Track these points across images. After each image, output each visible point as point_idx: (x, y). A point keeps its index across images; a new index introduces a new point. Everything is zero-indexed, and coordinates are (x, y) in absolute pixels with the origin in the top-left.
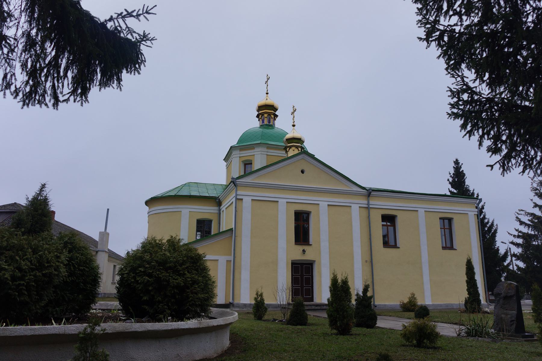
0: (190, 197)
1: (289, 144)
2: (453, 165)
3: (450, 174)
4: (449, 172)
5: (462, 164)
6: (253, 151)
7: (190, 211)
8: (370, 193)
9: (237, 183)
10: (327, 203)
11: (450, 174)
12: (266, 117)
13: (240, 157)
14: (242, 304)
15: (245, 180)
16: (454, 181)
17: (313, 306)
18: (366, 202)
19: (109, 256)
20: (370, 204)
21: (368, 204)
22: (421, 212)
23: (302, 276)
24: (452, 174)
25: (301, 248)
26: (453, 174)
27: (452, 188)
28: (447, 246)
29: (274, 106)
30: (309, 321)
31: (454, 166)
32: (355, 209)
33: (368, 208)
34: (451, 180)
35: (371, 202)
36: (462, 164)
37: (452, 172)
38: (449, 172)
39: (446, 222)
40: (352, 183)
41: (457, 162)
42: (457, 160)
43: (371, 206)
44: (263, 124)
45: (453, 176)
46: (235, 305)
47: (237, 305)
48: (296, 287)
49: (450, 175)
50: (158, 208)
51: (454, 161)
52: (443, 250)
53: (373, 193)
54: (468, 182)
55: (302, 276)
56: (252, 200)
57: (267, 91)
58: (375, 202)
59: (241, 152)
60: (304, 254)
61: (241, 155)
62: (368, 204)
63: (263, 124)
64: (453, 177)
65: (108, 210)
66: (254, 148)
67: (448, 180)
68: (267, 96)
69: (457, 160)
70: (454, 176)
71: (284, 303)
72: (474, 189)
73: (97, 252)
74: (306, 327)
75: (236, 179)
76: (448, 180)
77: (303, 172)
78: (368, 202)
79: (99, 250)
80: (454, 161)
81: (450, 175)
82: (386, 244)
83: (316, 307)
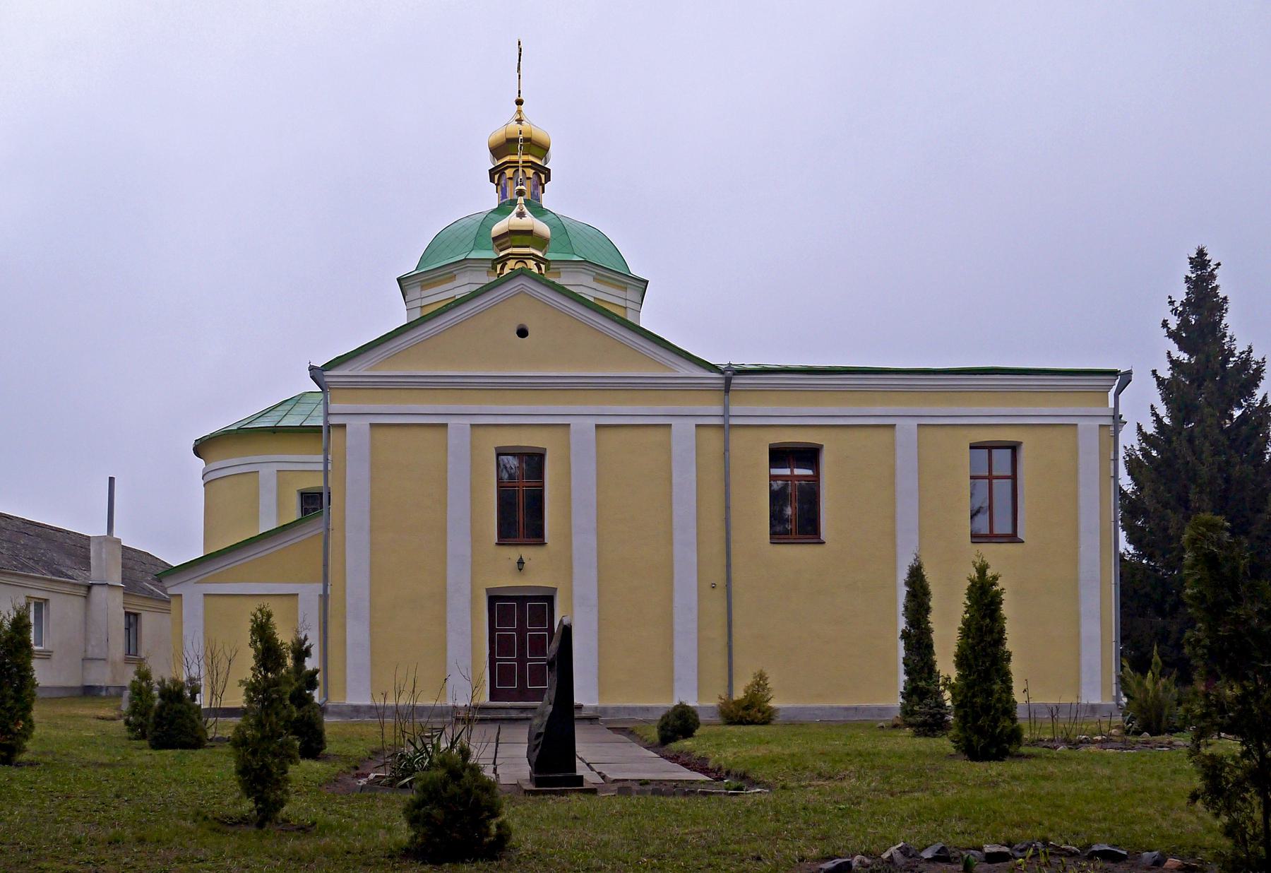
0: (274, 433)
1: (501, 251)
2: (1187, 270)
3: (1172, 303)
4: (1170, 297)
5: (1219, 264)
6: (622, 294)
7: (277, 471)
8: (728, 382)
9: (327, 380)
10: (593, 422)
11: (1172, 303)
12: (510, 178)
13: (421, 307)
14: (348, 706)
15: (350, 371)
16: (1184, 324)
17: (511, 711)
18: (718, 409)
19: (124, 593)
20: (730, 414)
21: (725, 415)
22: (907, 428)
23: (522, 631)
24: (1177, 304)
25: (513, 553)
26: (1182, 304)
27: (1180, 349)
28: (997, 531)
29: (533, 138)
30: (329, 749)
31: (1190, 275)
32: (683, 430)
33: (725, 428)
34: (1174, 323)
35: (734, 409)
36: (1219, 264)
37: (1181, 295)
38: (1170, 297)
39: (1002, 457)
40: (674, 352)
41: (1200, 261)
42: (1201, 253)
43: (733, 421)
44: (504, 200)
45: (1180, 309)
46: (330, 709)
47: (335, 709)
48: (509, 660)
49: (1171, 307)
50: (231, 462)
51: (1190, 258)
52: (772, 545)
53: (738, 380)
54: (1232, 322)
55: (522, 631)
56: (371, 425)
57: (519, 96)
58: (744, 409)
59: (425, 293)
60: (520, 570)
61: (425, 302)
62: (725, 415)
63: (504, 200)
64: (1181, 314)
65: (111, 480)
66: (453, 278)
67: (1165, 324)
68: (519, 112)
69: (1201, 253)
70: (1184, 309)
71: (461, 704)
72: (1250, 347)
73: (89, 587)
74: (1017, 767)
75: (323, 368)
76: (1165, 324)
77: (522, 333)
78: (726, 408)
79: (94, 582)
80: (1190, 258)
81: (1171, 307)
82: (780, 531)
83: (522, 712)
